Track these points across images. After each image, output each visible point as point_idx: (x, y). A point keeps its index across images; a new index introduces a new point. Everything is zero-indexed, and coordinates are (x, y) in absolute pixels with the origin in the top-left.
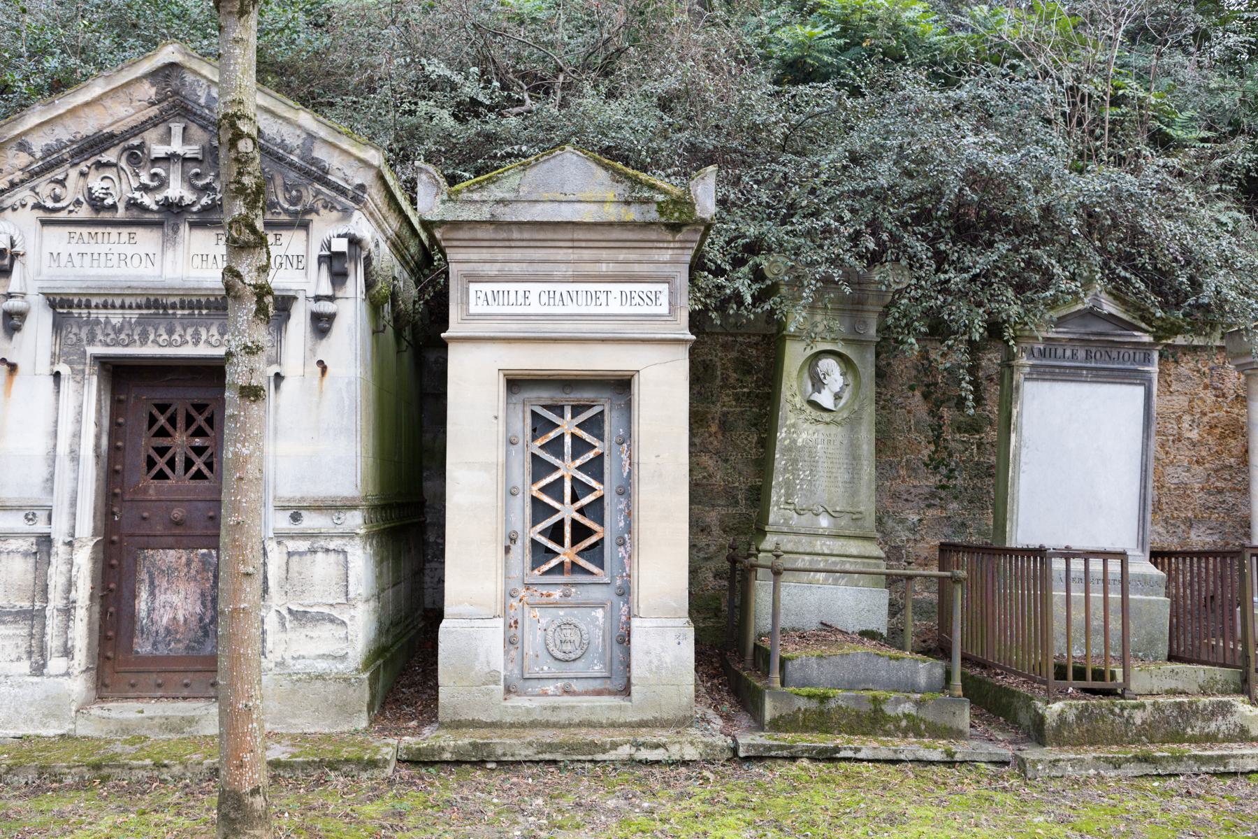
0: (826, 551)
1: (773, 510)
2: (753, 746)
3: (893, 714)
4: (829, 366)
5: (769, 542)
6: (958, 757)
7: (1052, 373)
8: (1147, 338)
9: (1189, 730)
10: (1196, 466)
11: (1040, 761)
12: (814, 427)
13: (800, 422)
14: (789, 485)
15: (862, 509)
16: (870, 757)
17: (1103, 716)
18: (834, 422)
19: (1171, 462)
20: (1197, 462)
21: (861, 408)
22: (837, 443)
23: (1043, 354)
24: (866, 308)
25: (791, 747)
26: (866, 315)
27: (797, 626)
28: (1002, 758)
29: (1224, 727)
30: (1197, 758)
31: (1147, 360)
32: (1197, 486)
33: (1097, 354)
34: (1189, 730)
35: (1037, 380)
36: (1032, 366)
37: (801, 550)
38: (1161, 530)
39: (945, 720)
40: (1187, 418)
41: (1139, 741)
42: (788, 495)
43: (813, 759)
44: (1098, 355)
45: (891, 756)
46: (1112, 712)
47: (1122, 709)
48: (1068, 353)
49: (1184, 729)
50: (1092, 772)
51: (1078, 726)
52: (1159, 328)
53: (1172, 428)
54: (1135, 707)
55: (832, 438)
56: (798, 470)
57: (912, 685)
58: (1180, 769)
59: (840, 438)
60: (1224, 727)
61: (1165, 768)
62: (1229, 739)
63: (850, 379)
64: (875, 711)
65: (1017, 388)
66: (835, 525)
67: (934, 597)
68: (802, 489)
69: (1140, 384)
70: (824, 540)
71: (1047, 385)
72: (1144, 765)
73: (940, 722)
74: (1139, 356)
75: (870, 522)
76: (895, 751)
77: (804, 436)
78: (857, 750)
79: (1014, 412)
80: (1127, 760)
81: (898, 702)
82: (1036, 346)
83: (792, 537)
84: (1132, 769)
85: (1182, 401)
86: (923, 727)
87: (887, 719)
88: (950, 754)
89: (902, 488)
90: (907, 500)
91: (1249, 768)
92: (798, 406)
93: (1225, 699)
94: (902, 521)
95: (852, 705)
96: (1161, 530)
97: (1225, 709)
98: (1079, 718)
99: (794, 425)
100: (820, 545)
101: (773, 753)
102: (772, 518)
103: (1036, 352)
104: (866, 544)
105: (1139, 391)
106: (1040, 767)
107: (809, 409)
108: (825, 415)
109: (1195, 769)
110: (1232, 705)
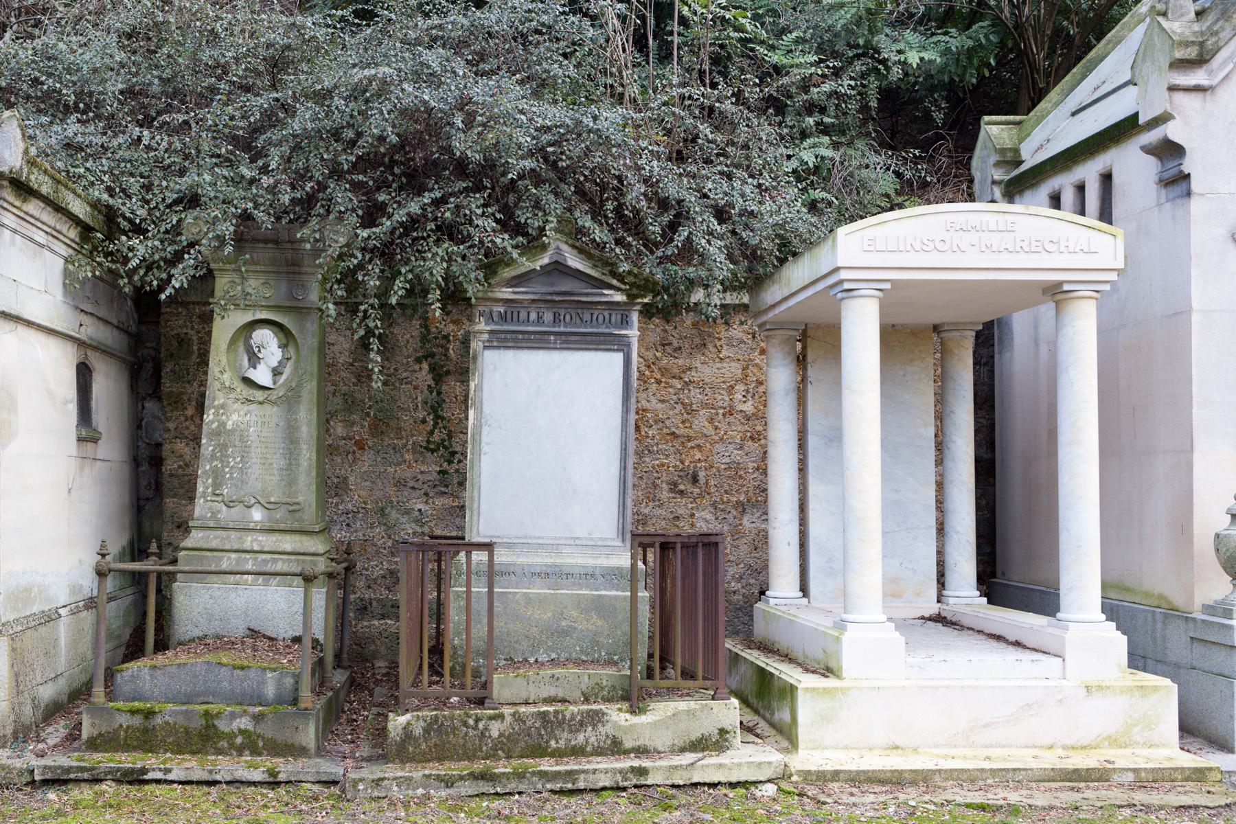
0: (256, 548)
1: (199, 502)
2: (50, 767)
3: (227, 730)
4: (266, 339)
5: (195, 538)
6: (282, 777)
7: (515, 340)
8: (619, 297)
9: (553, 743)
10: (750, 443)
11: (361, 780)
12: (246, 408)
13: (229, 402)
14: (217, 475)
15: (301, 499)
16: (182, 778)
17: (454, 728)
19: (721, 439)
20: (752, 438)
21: (300, 385)
22: (273, 425)
23: (503, 318)
24: (303, 269)
25: (93, 769)
26: (305, 277)
27: (222, 633)
28: (332, 778)
29: (593, 739)
30: (543, 775)
31: (625, 322)
32: (751, 465)
33: (567, 318)
34: (553, 743)
35: (498, 348)
36: (491, 332)
37: (227, 547)
38: (708, 517)
39: (286, 736)
40: (740, 388)
41: (494, 756)
42: (216, 485)
43: (119, 781)
44: (568, 317)
45: (205, 776)
46: (465, 724)
47: (477, 720)
48: (533, 316)
49: (547, 742)
50: (420, 791)
51: (426, 740)
52: (632, 285)
53: (723, 399)
54: (491, 718)
56: (228, 456)
57: (259, 697)
58: (522, 787)
59: (275, 419)
60: (593, 739)
61: (505, 786)
62: (599, 752)
63: (291, 350)
64: (207, 727)
65: (475, 358)
66: (270, 519)
67: (629, 594)
68: (232, 478)
69: (618, 350)
71: (510, 354)
72: (481, 783)
73: (280, 739)
74: (616, 317)
75: (310, 513)
76: (210, 772)
77: (235, 417)
78: (168, 771)
80: (462, 778)
81: (233, 716)
82: (495, 309)
83: (220, 533)
84: (467, 788)
85: (735, 369)
86: (261, 744)
87: (221, 735)
88: (272, 773)
89: (408, 474)
90: (413, 488)
91: (601, 784)
92: (227, 384)
93: (595, 707)
94: (408, 512)
95: (181, 721)
96: (708, 517)
97: (596, 718)
98: (427, 731)
99: (222, 406)
100: (250, 541)
101: (72, 776)
103: (495, 314)
104: (304, 538)
105: (618, 358)
106: (361, 787)
108: (260, 396)
109: (539, 786)
110: (604, 714)
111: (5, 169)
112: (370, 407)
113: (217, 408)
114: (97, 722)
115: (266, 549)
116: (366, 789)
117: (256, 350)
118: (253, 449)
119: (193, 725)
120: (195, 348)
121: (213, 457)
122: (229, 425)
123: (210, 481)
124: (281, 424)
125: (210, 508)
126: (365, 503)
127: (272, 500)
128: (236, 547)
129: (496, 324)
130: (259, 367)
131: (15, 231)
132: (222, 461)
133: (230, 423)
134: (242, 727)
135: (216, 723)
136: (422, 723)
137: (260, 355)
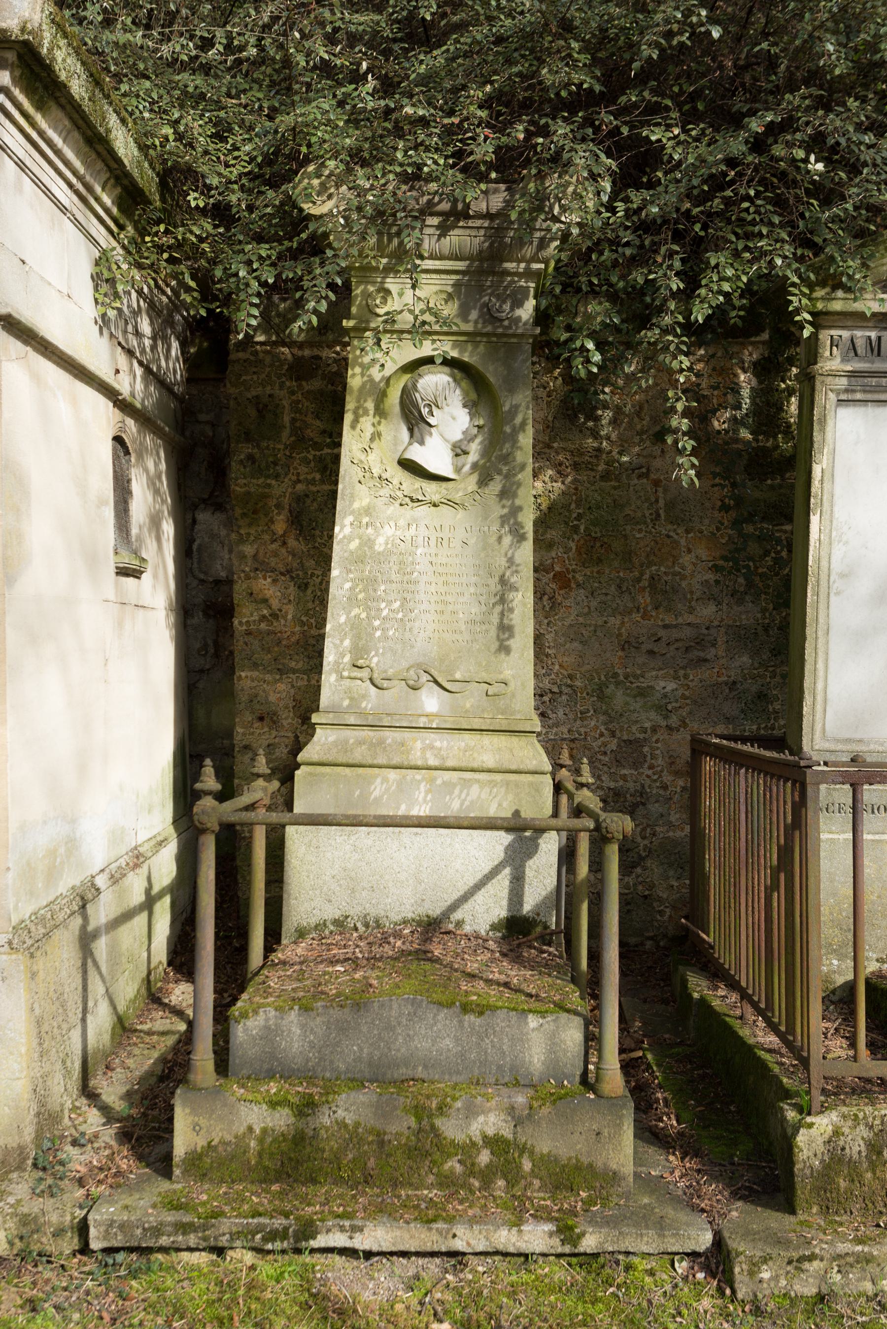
0: (432, 762)
3: (460, 1137)
18: (451, 503)
22: (457, 544)
36: (853, 375)
55: (446, 534)
56: (378, 599)
59: (460, 534)
70: (431, 737)
77: (389, 531)
79: (817, 470)
90: (651, 653)
92: (376, 471)
99: (368, 511)
101: (164, 1241)
102: (326, 697)
107: (399, 475)
108: (432, 490)
111: (12, 24)
112: (579, 517)
113: (358, 514)
114: (203, 1122)
115: (450, 763)
116: (776, 1278)
117: (425, 411)
118: (422, 587)
119: (393, 1128)
120: (287, 419)
121: (352, 600)
122: (380, 545)
123: (347, 643)
124: (472, 541)
125: (348, 691)
126: (571, 677)
127: (458, 676)
128: (396, 761)
129: (863, 359)
130: (428, 440)
131: (21, 165)
132: (368, 609)
133: (381, 540)
134: (490, 1132)
135: (438, 1122)
136: (863, 1131)
137: (431, 420)
